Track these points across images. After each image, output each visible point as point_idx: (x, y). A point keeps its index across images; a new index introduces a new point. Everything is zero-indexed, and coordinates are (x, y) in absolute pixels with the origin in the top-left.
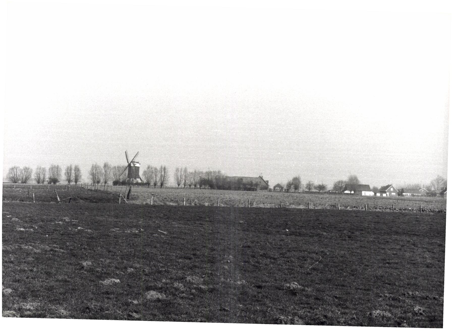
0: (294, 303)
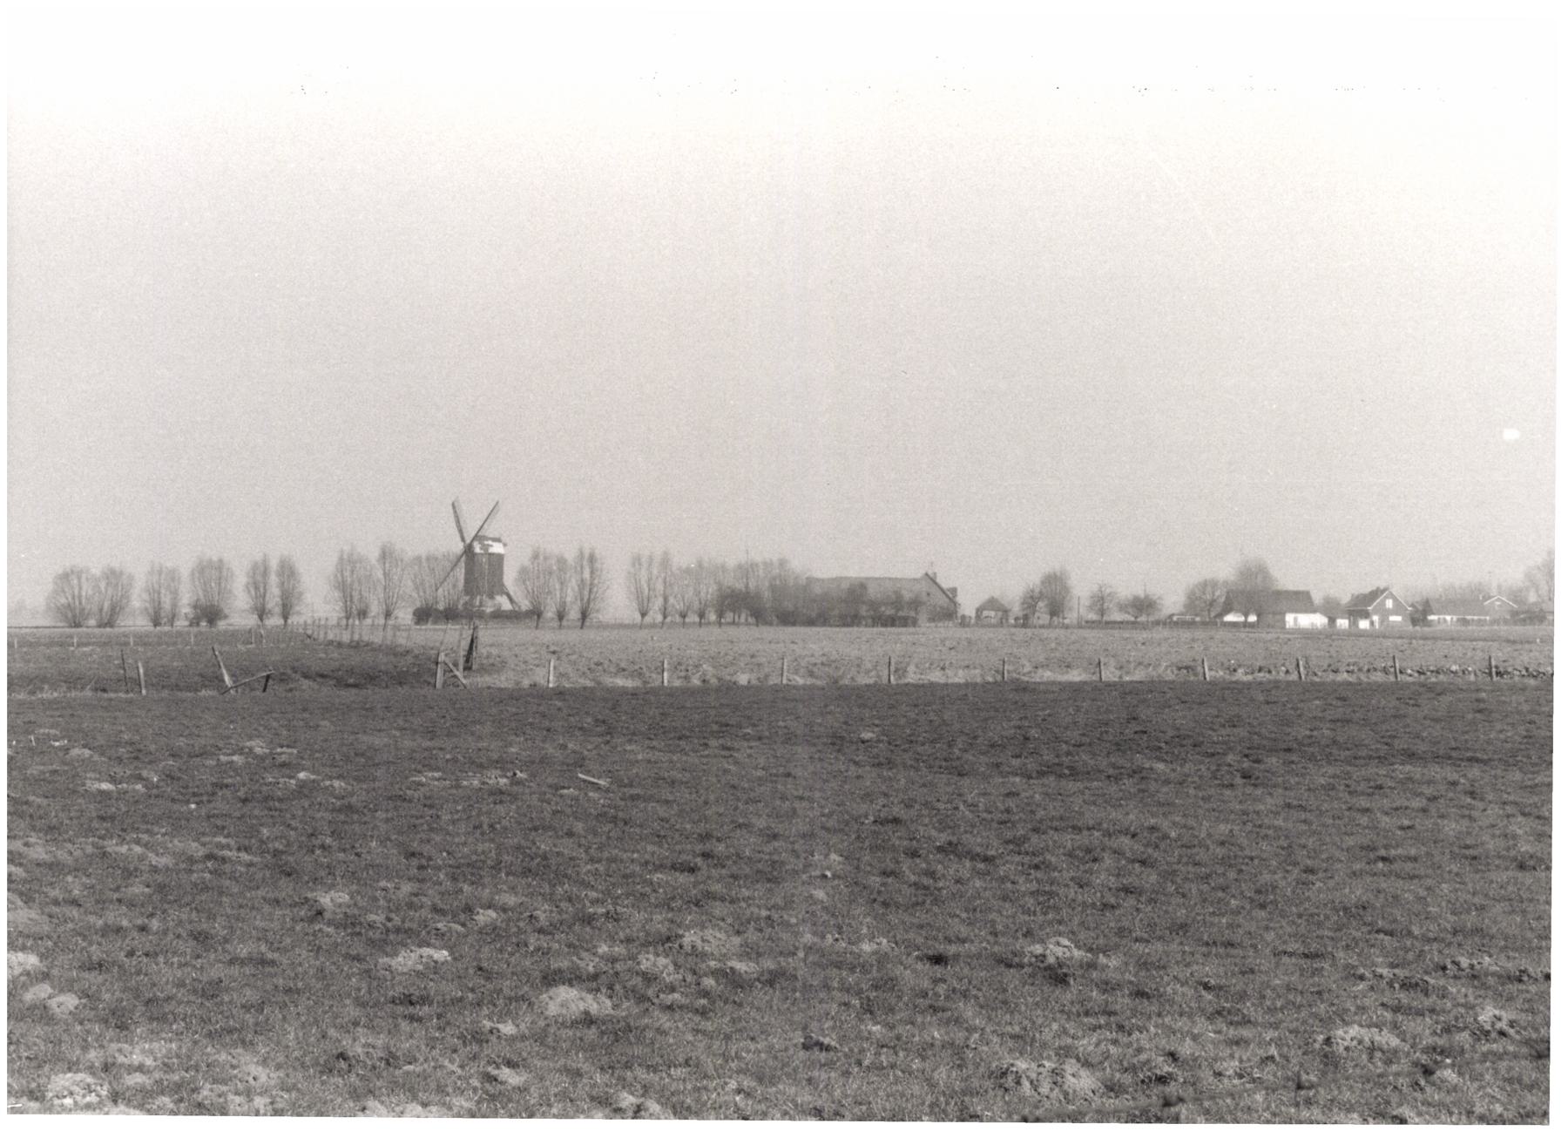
0: (1062, 1011)
